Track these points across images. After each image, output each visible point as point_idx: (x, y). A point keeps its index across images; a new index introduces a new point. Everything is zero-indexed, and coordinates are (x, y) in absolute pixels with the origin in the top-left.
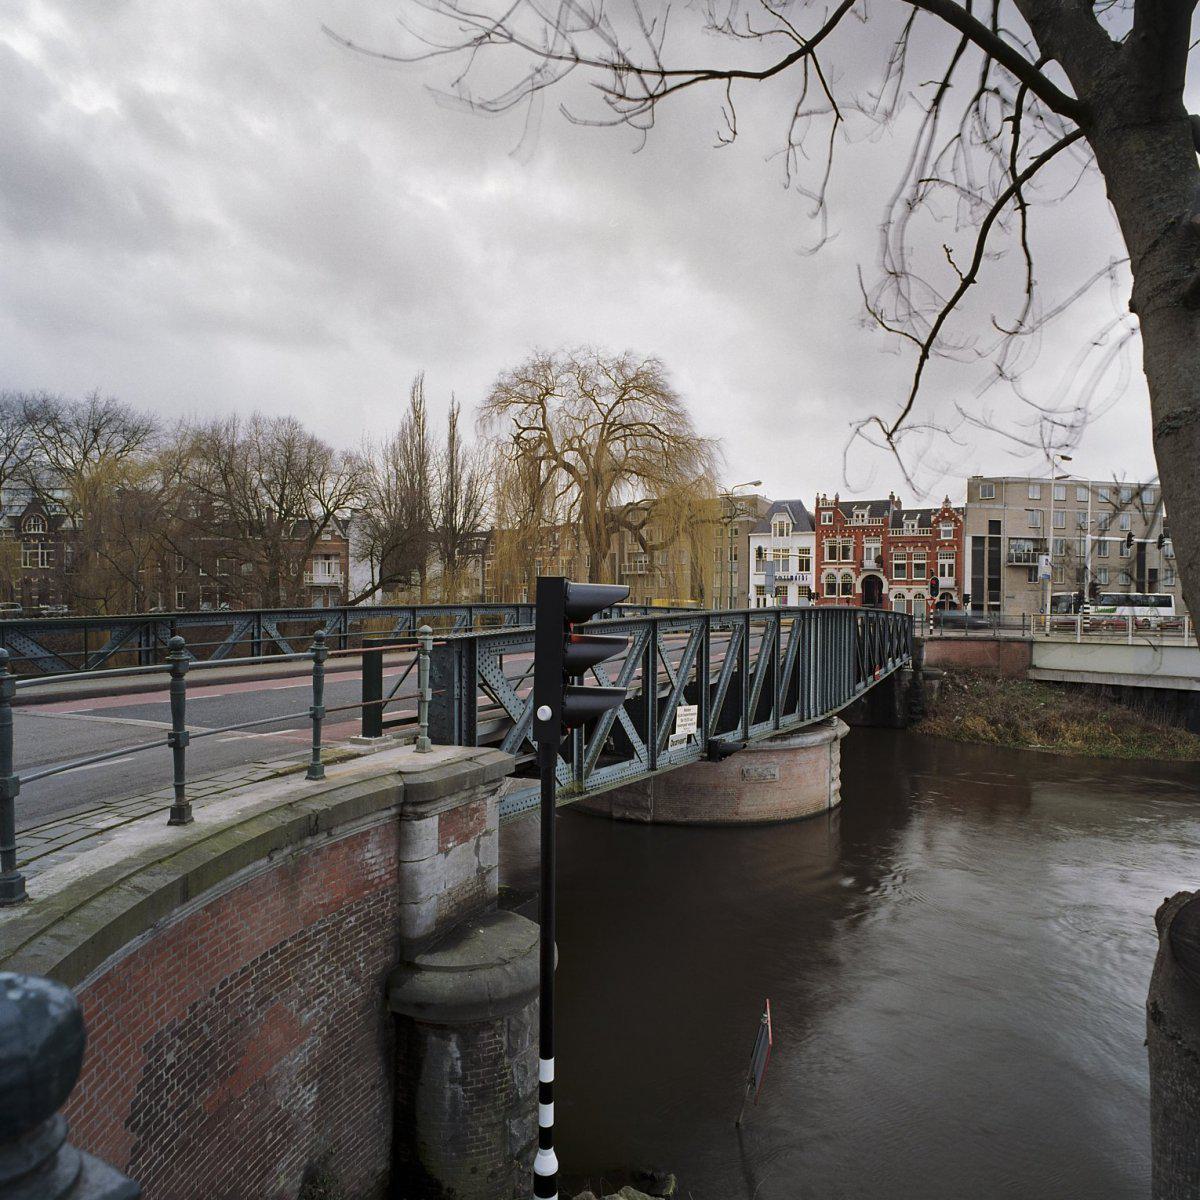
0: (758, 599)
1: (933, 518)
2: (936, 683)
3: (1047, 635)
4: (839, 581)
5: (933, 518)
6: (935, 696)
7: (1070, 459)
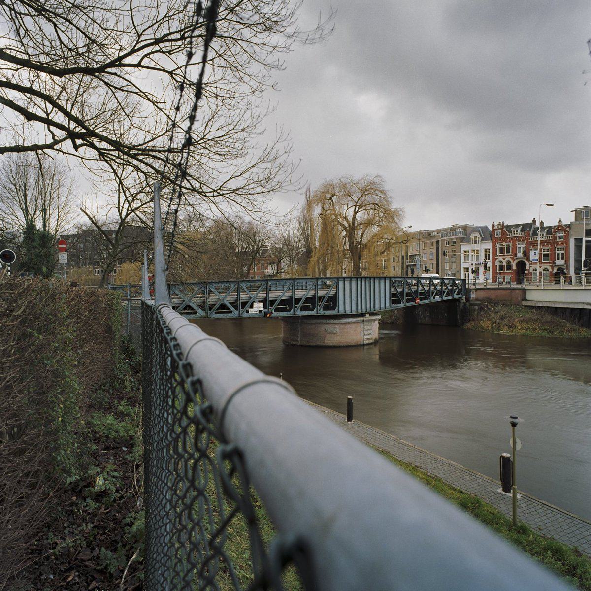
0: (465, 274)
1: (553, 230)
2: (476, 307)
3: (538, 286)
4: (504, 264)
5: (553, 230)
6: (476, 313)
7: (553, 205)
